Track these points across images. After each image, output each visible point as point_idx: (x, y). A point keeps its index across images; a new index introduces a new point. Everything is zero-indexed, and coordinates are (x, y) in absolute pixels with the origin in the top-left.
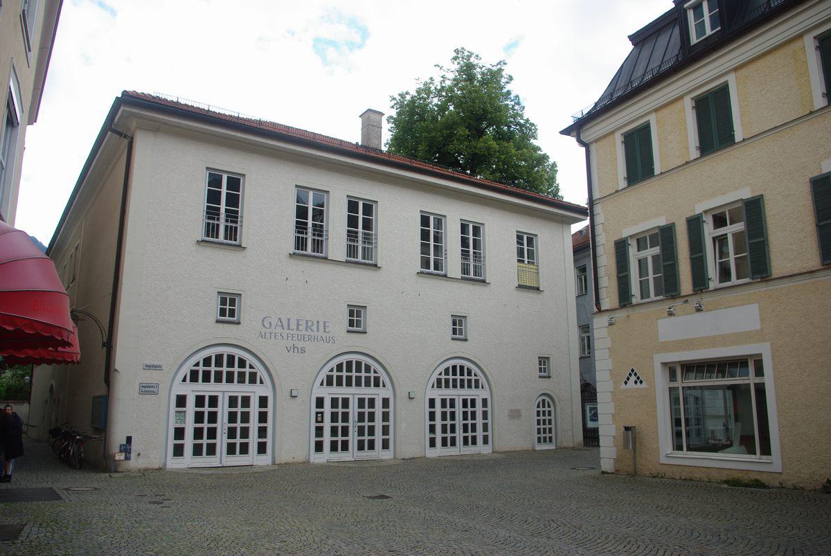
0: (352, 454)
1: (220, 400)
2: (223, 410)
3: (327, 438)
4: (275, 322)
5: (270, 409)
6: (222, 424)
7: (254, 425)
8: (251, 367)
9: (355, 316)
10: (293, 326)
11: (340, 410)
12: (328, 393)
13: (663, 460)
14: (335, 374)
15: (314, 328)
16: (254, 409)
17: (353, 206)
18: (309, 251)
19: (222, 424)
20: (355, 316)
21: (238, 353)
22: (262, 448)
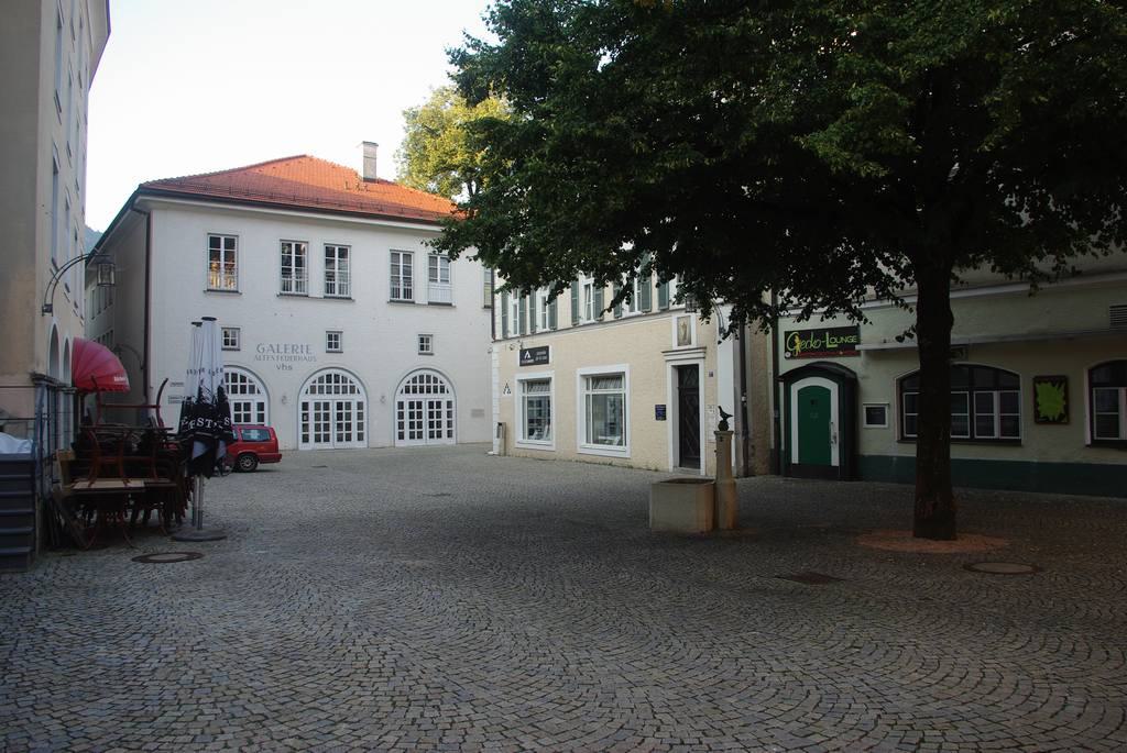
0: (333, 444)
1: (331, 405)
2: (425, 410)
3: (312, 433)
4: (267, 347)
5: (266, 412)
6: (425, 420)
7: (444, 419)
8: (250, 381)
9: (333, 340)
10: (282, 350)
11: (243, 412)
12: (312, 399)
13: (580, 451)
14: (411, 384)
15: (299, 350)
16: (444, 409)
17: (329, 252)
18: (294, 291)
19: (425, 420)
20: (333, 340)
21: (433, 374)
22: (360, 437)
